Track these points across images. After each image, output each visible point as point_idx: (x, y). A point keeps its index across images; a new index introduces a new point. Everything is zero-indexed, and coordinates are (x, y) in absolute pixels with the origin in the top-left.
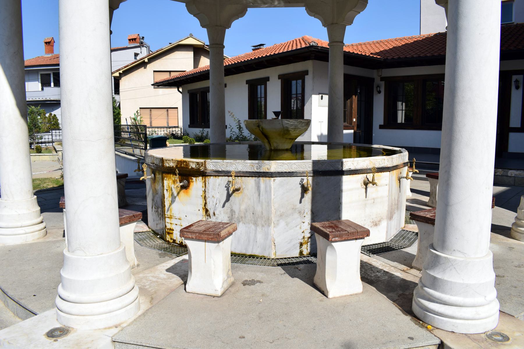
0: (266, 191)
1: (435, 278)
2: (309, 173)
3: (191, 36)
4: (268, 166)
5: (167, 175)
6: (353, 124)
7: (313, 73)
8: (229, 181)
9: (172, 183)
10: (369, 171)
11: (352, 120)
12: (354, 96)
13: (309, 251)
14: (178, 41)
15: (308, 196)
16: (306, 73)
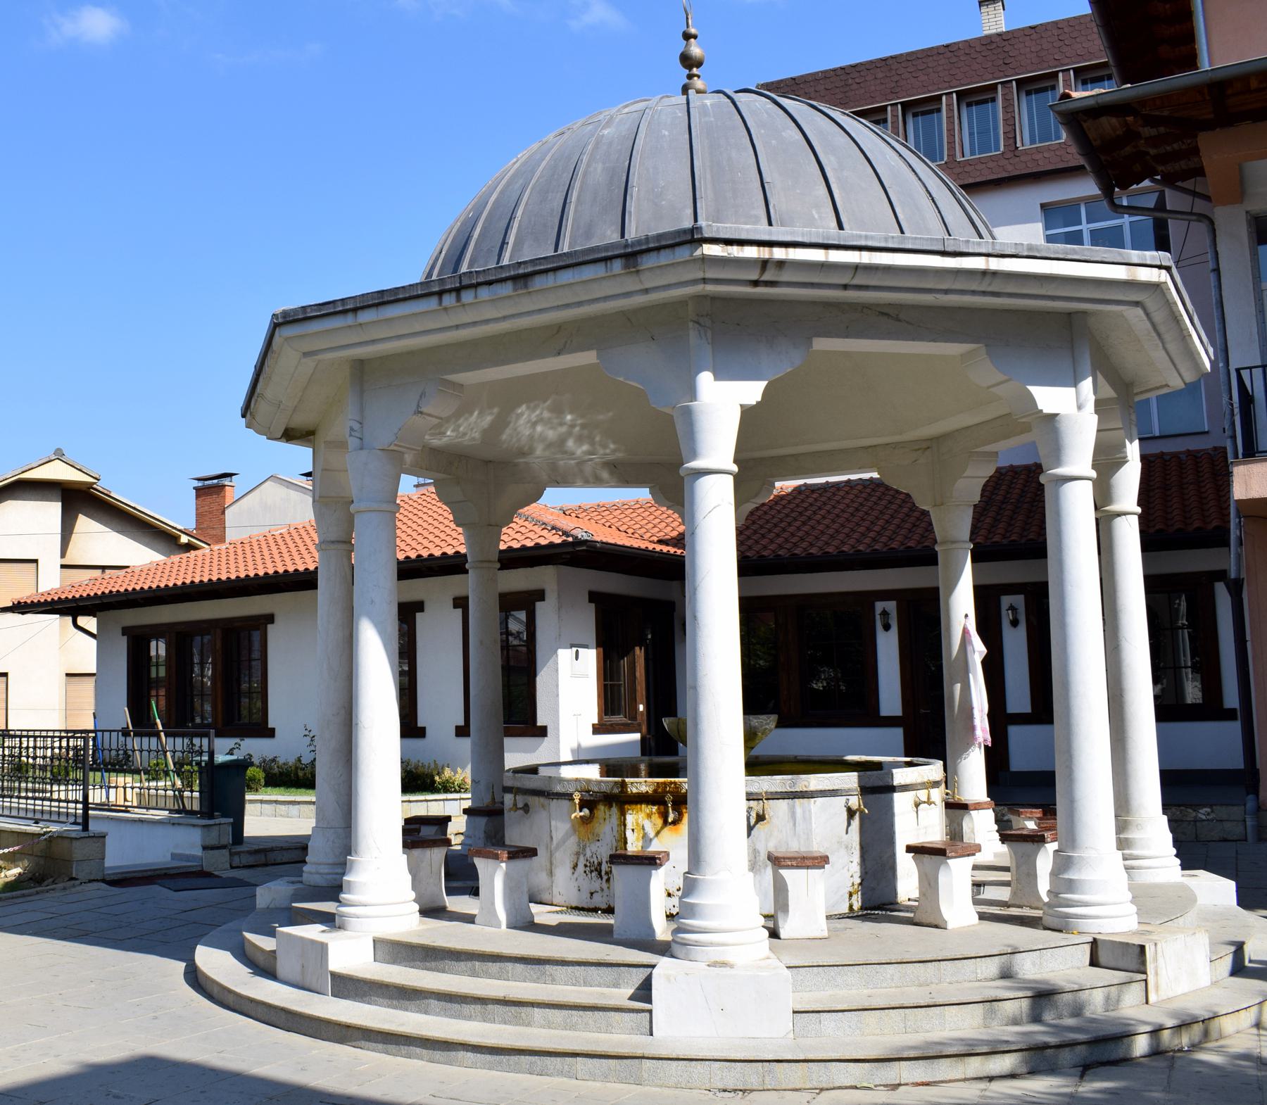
0: (804, 818)
1: (1071, 881)
2: (856, 790)
3: (59, 455)
4: (806, 783)
5: (634, 806)
6: (639, 717)
7: (559, 597)
8: (749, 808)
9: (645, 817)
10: (919, 787)
11: (636, 709)
12: (637, 649)
13: (860, 904)
14: (20, 471)
15: (856, 822)
16: (540, 595)
